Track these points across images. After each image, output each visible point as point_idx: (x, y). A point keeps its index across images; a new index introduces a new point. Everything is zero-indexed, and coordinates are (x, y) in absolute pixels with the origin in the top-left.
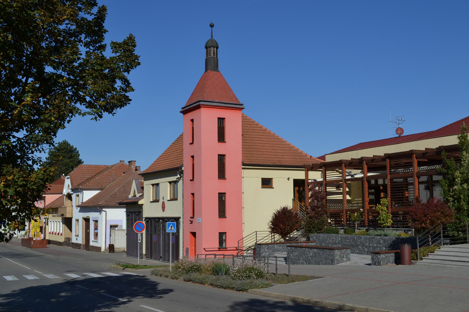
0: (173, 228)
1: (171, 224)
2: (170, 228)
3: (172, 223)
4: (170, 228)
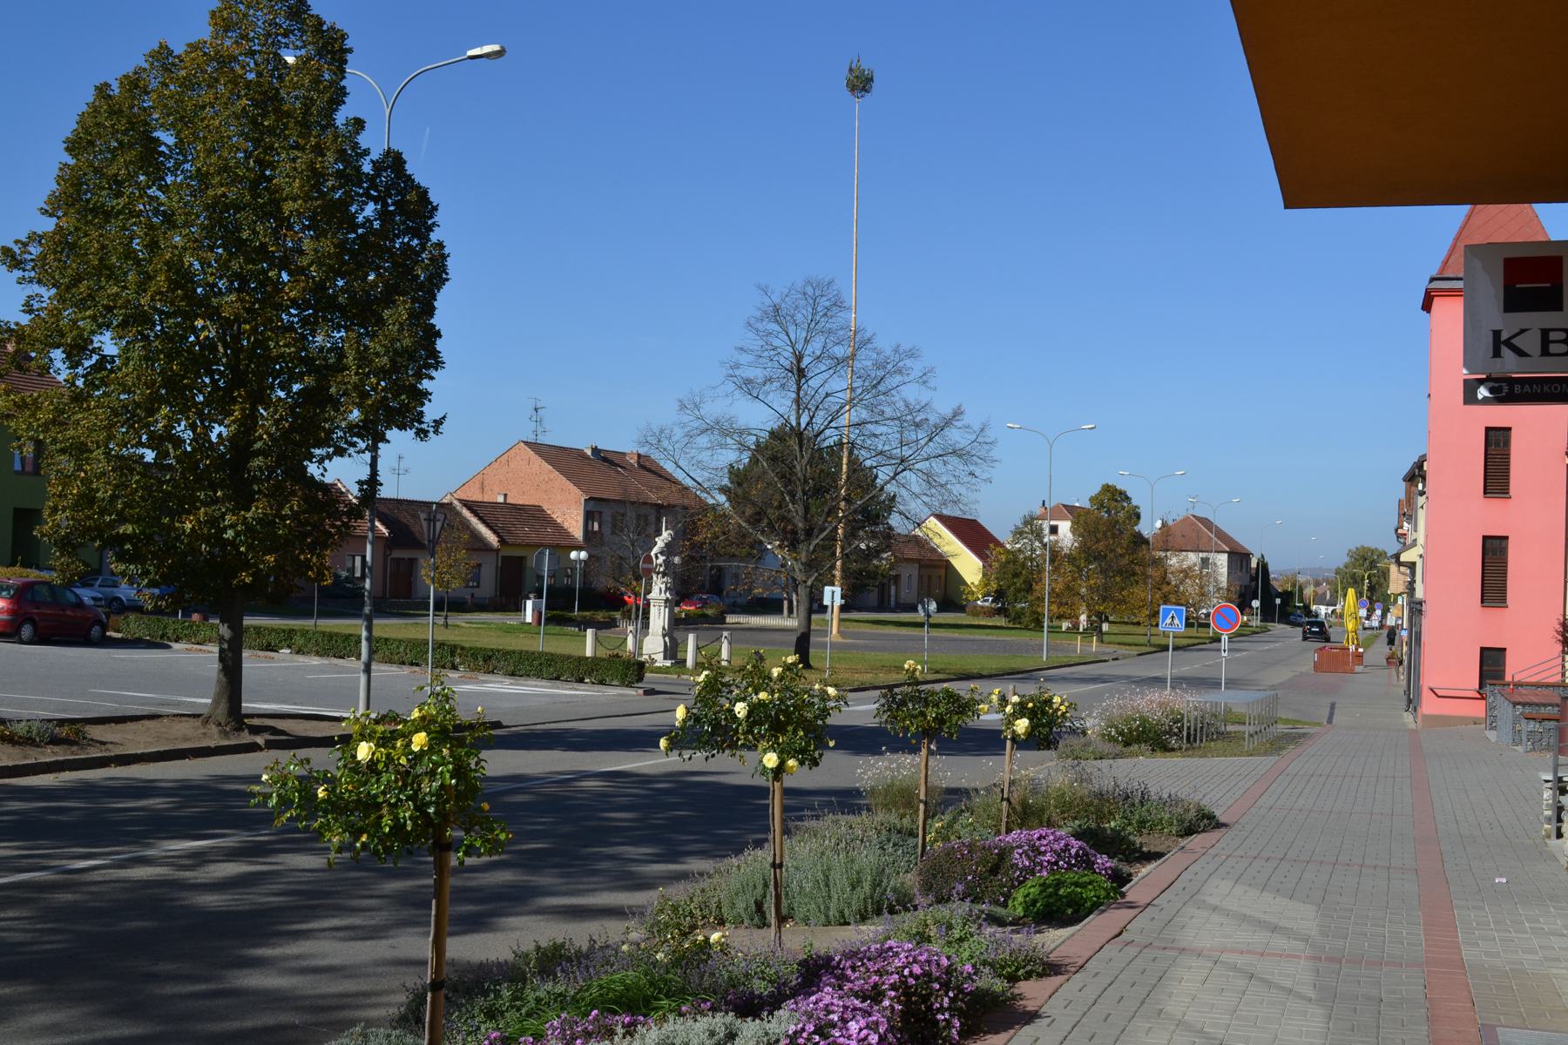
0: (1176, 621)
1: (1171, 610)
2: (1168, 621)
3: (1175, 610)
4: (1168, 621)
